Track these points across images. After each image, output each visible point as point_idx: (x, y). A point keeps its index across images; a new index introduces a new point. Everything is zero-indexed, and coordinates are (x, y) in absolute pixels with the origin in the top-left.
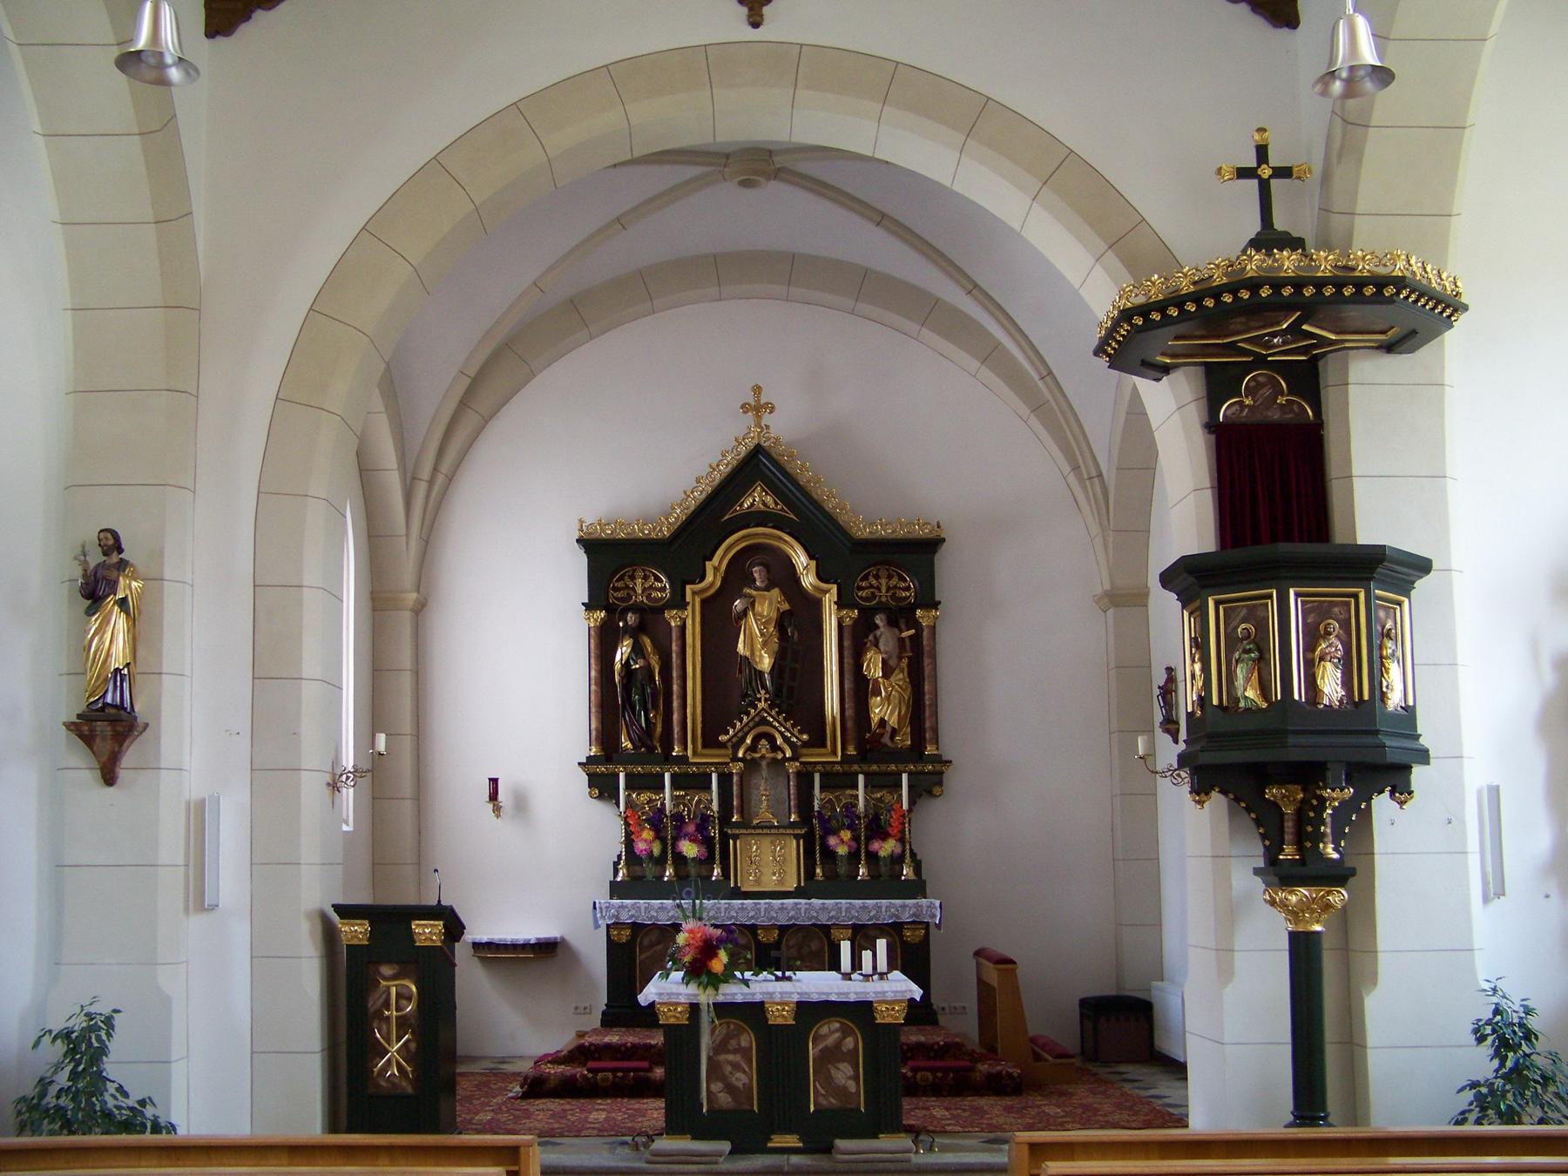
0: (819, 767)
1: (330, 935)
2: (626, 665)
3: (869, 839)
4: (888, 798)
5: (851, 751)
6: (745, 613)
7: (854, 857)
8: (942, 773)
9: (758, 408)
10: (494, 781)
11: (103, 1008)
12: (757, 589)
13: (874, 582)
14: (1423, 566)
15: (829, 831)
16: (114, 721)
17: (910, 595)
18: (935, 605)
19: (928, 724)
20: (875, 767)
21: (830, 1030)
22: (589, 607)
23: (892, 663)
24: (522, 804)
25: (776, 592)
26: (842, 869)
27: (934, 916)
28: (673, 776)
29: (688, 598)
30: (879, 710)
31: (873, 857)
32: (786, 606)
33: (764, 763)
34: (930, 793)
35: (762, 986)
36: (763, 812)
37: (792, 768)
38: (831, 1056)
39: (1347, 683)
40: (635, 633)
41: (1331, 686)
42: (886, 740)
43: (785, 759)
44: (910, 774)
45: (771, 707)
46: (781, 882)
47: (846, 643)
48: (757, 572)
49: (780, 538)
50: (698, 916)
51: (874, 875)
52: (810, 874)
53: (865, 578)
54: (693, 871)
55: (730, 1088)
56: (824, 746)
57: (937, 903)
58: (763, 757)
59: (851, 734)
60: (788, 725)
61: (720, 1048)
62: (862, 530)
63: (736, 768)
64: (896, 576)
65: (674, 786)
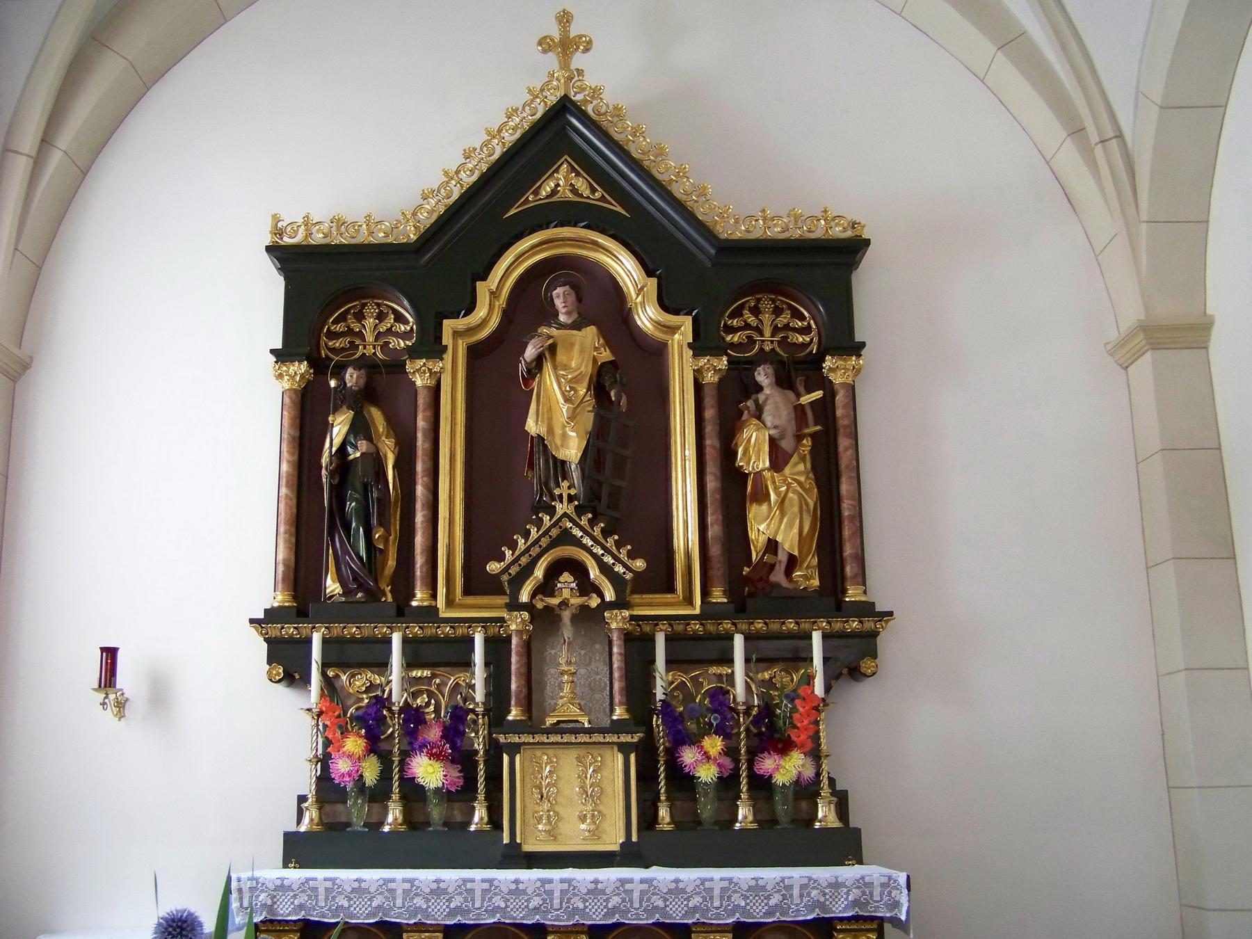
0: (664, 625)
3: (753, 754)
5: (718, 596)
6: (538, 364)
7: (728, 783)
8: (874, 635)
9: (566, 45)
10: (110, 654)
12: (562, 326)
13: (752, 320)
15: (681, 738)
17: (812, 341)
18: (856, 349)
19: (848, 550)
20: (759, 625)
22: (281, 356)
23: (787, 444)
24: (161, 695)
25: (590, 332)
26: (707, 809)
27: (896, 904)
28: (405, 641)
29: (447, 339)
30: (762, 525)
31: (762, 786)
32: (606, 355)
33: (566, 615)
36: (564, 705)
37: (616, 621)
42: (778, 576)
43: (605, 606)
45: (580, 510)
46: (595, 834)
47: (709, 413)
48: (561, 298)
49: (595, 243)
51: (766, 821)
52: (648, 819)
53: (737, 313)
54: (436, 812)
56: (671, 589)
57: (902, 878)
58: (565, 604)
59: (718, 570)
60: (610, 543)
64: (789, 297)
65: (410, 662)
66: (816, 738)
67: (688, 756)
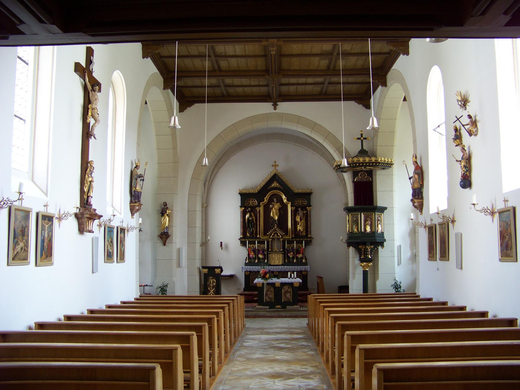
1: (200, 272)
2: (248, 219)
4: (301, 246)
5: (293, 236)
7: (293, 258)
9: (275, 166)
10: (221, 243)
11: (166, 283)
14: (386, 208)
15: (289, 252)
16: (166, 235)
17: (306, 204)
18: (310, 206)
21: (286, 288)
22: (241, 207)
24: (227, 247)
25: (279, 204)
26: (291, 260)
30: (299, 228)
31: (297, 258)
34: (309, 245)
35: (275, 280)
36: (275, 248)
37: (281, 240)
38: (286, 292)
39: (371, 229)
40: (250, 212)
41: (368, 229)
42: (300, 234)
44: (305, 241)
50: (262, 270)
51: (297, 261)
52: (285, 261)
54: (261, 260)
55: (269, 298)
61: (267, 291)
62: (296, 191)
63: (270, 240)
64: (303, 200)
65: (258, 243)
66: (166, 241)
67: (289, 254)
